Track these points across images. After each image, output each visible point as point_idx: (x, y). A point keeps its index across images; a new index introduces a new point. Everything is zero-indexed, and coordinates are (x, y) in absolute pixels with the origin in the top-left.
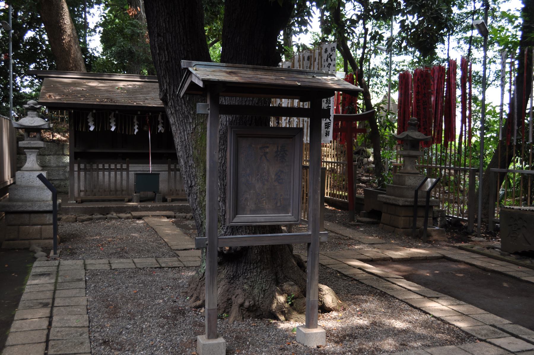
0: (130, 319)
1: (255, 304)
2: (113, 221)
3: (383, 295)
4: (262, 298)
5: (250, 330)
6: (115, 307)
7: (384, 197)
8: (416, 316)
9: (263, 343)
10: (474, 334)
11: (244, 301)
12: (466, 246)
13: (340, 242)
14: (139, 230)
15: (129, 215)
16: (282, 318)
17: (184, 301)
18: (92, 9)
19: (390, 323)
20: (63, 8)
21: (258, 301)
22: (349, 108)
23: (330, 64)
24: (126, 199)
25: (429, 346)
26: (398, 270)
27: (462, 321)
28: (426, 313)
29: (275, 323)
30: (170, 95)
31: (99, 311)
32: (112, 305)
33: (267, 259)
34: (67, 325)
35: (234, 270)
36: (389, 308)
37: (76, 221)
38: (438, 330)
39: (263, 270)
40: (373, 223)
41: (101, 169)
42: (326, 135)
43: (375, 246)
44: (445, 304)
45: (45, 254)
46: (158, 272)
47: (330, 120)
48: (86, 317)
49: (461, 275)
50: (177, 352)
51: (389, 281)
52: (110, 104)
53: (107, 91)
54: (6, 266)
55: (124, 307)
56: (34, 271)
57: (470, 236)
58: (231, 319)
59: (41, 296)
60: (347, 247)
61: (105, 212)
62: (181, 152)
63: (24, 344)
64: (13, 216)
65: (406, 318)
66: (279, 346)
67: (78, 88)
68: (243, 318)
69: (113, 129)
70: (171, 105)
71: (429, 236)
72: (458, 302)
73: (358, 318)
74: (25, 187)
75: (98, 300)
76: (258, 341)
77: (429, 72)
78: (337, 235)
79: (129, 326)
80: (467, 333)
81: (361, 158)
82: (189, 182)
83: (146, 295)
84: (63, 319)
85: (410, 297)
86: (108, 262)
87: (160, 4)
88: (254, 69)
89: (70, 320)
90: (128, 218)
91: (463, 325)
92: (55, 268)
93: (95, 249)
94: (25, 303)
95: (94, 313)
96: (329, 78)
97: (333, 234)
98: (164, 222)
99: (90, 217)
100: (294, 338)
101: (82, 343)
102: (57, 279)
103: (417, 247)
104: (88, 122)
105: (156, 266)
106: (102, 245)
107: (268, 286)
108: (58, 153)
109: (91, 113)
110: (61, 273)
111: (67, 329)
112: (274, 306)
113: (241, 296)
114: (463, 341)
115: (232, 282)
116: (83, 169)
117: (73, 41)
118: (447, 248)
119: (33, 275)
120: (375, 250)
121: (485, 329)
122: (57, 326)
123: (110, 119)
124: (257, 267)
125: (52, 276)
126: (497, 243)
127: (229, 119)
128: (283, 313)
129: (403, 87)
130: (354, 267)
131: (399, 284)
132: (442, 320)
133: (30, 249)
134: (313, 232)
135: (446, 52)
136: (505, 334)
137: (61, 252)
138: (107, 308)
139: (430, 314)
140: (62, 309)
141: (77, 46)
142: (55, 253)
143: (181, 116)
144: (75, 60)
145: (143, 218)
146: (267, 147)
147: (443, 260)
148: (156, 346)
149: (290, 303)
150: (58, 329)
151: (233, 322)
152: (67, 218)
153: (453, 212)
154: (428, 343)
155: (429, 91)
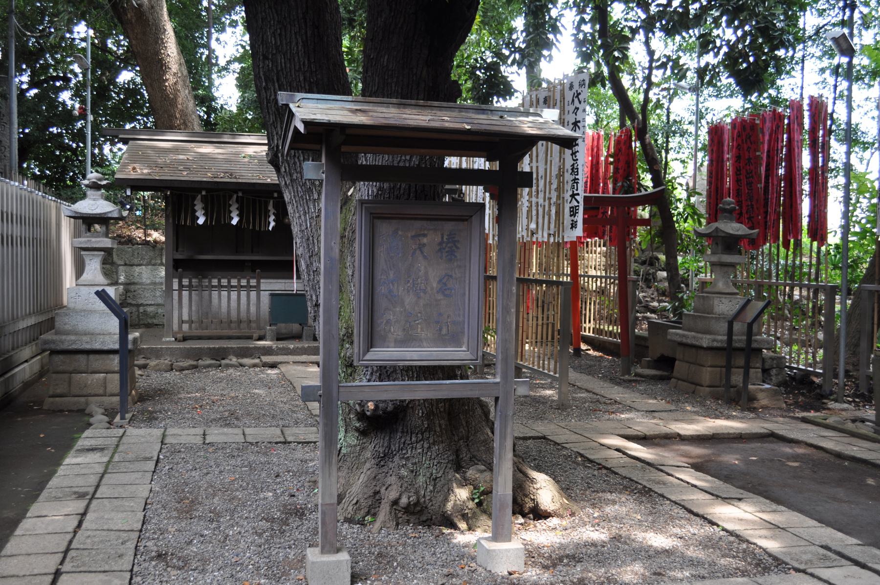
0: (211, 521)
1: (418, 501)
2: (231, 370)
3: (645, 493)
4: (431, 492)
5: (404, 545)
6: (192, 501)
7: (677, 334)
8: (695, 529)
9: (420, 565)
10: (787, 560)
11: (400, 495)
12: (815, 417)
13: (599, 406)
14: (268, 385)
15: (257, 361)
16: (463, 525)
17: (308, 495)
18: (224, 34)
19: (644, 539)
20: (165, 30)
21: (424, 496)
22: (623, 186)
23: (577, 109)
24: (255, 336)
25: (704, 577)
26: (686, 455)
27: (773, 538)
28: (712, 523)
29: (449, 534)
30: (283, 155)
31: (164, 507)
32: (188, 499)
33: (440, 426)
34: (105, 527)
35: (386, 444)
36: (651, 513)
37: (172, 370)
38: (727, 551)
39: (434, 444)
40: (661, 379)
41: (215, 287)
42: (572, 228)
43: (656, 414)
44: (750, 509)
45: (106, 419)
46: (281, 451)
47: (578, 202)
48: (140, 515)
49: (796, 464)
50: (275, 575)
51: (662, 471)
52: (228, 180)
53: (227, 161)
54: (42, 436)
55: (207, 502)
56: (81, 443)
57: (825, 401)
58: (377, 525)
59: (80, 481)
60: (607, 416)
61: (219, 355)
62: (301, 249)
63: (29, 555)
64: (61, 357)
65: (677, 530)
66: (446, 571)
67: (181, 157)
68: (397, 524)
69: (235, 222)
70: (285, 171)
71: (752, 398)
72: (774, 506)
73: (593, 529)
74: (81, 311)
75: (167, 491)
76: (413, 561)
77: (758, 122)
78: (595, 396)
79: (206, 532)
80: (775, 559)
81: (651, 271)
82: (314, 297)
83: (248, 484)
84: (102, 518)
85: (692, 497)
86: (202, 433)
87: (267, 6)
88: (399, 105)
89: (112, 519)
90: (255, 366)
91: (772, 545)
92: (115, 441)
93: (188, 413)
94: (50, 493)
95: (156, 510)
96: (531, 118)
97: (591, 395)
98: (312, 372)
99: (195, 363)
100: (473, 558)
101: (121, 556)
102: (112, 457)
103: (728, 418)
104: (195, 211)
105: (278, 440)
106: (201, 406)
107: (441, 472)
108: (153, 262)
109: (199, 196)
110: (121, 448)
111: (105, 533)
112: (449, 506)
113: (395, 487)
114: (766, 570)
115: (382, 463)
116: (186, 287)
117: (181, 83)
118: (781, 419)
119: (78, 450)
120: (654, 421)
121: (810, 552)
122: (89, 527)
123: (230, 205)
124: (422, 440)
125: (106, 452)
126: (870, 413)
127: (372, 191)
128: (465, 517)
129: (715, 149)
130: (609, 447)
131: (678, 476)
132: (737, 536)
133: (86, 412)
134: (502, 378)
135: (799, 91)
136: (844, 562)
137: (133, 415)
138: (179, 503)
139: (718, 526)
140: (106, 502)
141: (187, 91)
142: (123, 418)
143: (300, 189)
144: (184, 114)
145: (279, 366)
146: (425, 235)
147: (771, 439)
148: (242, 564)
149: (477, 501)
150: (89, 533)
151: (381, 531)
152: (157, 365)
153: (801, 359)
154: (703, 572)
155: (758, 153)
